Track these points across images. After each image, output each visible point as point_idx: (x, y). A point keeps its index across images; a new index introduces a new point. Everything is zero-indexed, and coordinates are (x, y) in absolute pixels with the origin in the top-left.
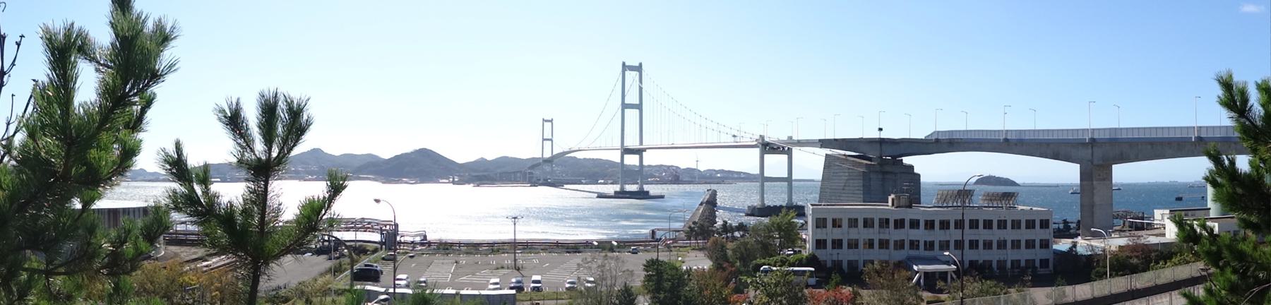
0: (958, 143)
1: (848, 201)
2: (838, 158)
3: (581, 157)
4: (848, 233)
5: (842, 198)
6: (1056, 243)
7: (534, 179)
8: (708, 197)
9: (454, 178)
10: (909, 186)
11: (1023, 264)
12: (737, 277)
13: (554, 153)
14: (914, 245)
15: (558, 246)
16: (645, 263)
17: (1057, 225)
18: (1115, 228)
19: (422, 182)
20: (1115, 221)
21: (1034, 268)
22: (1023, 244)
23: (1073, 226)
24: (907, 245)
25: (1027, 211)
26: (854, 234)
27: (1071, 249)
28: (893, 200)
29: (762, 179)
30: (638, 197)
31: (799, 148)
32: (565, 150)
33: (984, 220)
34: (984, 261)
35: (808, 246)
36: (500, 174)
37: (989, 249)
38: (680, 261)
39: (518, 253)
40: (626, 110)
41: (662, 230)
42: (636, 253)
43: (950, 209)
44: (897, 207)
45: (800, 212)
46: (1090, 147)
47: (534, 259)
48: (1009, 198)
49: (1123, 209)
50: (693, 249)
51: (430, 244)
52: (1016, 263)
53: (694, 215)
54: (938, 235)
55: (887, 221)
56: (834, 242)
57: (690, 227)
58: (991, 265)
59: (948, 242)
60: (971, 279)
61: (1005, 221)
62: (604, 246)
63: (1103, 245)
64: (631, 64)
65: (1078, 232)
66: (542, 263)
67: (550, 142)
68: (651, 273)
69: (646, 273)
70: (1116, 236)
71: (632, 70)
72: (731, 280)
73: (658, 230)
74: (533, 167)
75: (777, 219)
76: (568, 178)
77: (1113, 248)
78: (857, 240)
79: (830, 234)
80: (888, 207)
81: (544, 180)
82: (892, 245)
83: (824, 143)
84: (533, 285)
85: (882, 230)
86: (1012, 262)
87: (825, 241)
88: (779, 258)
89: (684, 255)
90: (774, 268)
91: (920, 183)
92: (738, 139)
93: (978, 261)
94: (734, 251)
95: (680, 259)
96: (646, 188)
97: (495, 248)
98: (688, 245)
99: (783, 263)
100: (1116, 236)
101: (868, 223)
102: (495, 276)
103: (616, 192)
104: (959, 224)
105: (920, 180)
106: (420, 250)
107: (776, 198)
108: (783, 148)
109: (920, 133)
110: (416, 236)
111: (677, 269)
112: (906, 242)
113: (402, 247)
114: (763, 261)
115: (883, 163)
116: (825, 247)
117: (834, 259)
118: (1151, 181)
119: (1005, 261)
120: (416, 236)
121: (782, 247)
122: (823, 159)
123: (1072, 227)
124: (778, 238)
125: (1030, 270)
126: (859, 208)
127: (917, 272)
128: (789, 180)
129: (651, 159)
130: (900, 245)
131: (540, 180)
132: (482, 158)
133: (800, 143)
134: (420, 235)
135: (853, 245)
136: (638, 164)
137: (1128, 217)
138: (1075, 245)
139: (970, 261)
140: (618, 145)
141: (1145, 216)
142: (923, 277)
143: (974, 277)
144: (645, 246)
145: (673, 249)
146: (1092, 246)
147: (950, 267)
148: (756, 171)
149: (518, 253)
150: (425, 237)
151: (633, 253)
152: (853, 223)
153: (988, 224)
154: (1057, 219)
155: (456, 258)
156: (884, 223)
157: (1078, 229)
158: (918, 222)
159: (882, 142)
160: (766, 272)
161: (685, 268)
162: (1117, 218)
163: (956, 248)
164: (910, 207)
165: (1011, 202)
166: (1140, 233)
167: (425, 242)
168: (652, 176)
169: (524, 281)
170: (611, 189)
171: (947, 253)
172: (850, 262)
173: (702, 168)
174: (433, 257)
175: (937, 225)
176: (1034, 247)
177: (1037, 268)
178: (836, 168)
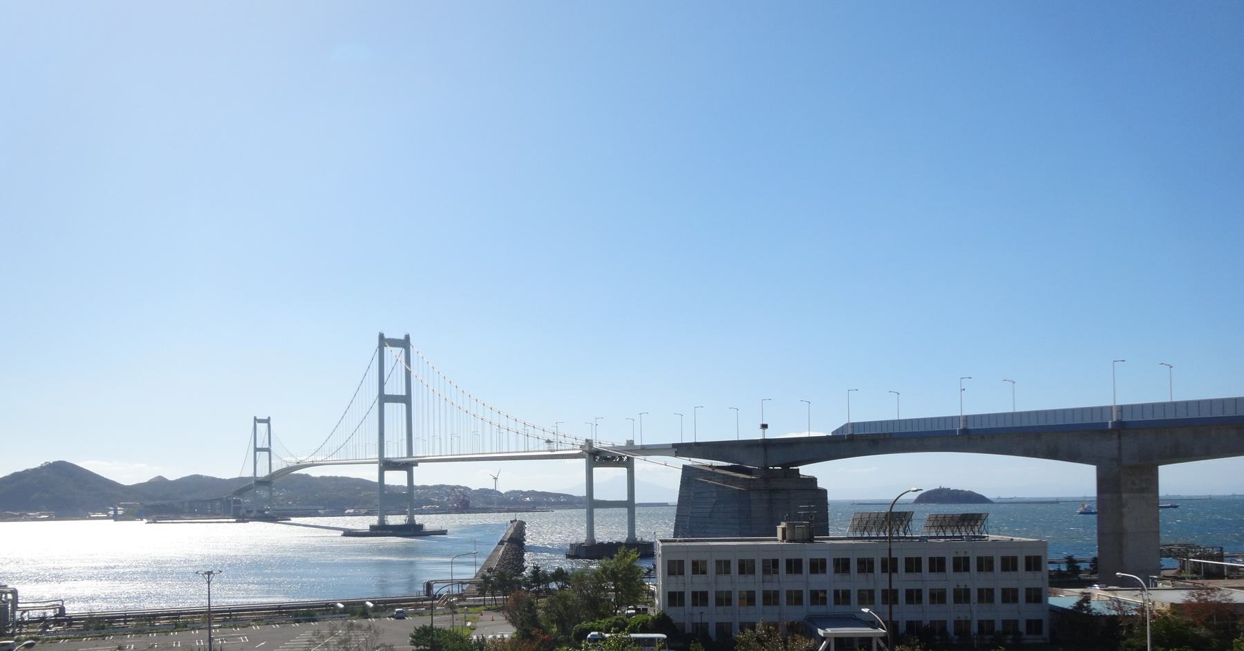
3: (304, 473)
6: (1055, 595)
7: (243, 511)
8: (511, 531)
10: (809, 509)
11: (998, 627)
13: (274, 470)
15: (280, 613)
16: (412, 631)
18: (1164, 573)
21: (1017, 633)
22: (998, 595)
23: (1083, 566)
24: (806, 598)
27: (1080, 604)
28: (784, 530)
29: (590, 504)
30: (409, 533)
31: (642, 457)
32: (290, 465)
33: (931, 559)
35: (657, 602)
37: (939, 603)
39: (215, 628)
40: (386, 405)
41: (442, 581)
42: (403, 618)
44: (790, 541)
45: (646, 550)
46: (1115, 436)
50: (489, 609)
51: (70, 621)
53: (490, 558)
54: (855, 582)
55: (775, 563)
59: (871, 592)
61: (967, 560)
63: (1140, 601)
67: (267, 453)
68: (422, 647)
70: (1166, 586)
71: (395, 346)
73: (436, 582)
74: (240, 492)
76: (299, 507)
78: (729, 593)
79: (690, 583)
80: (777, 541)
81: (259, 511)
83: (680, 449)
85: (768, 577)
86: (981, 623)
87: (682, 594)
90: (607, 635)
91: (827, 504)
92: (554, 446)
93: (921, 622)
95: (469, 624)
96: (419, 519)
99: (621, 626)
100: (1166, 586)
101: (746, 567)
104: (890, 565)
107: (610, 530)
108: (621, 457)
109: (822, 429)
111: (462, 640)
113: (24, 631)
115: (768, 475)
116: (682, 603)
118: (1237, 493)
119: (968, 622)
120: (47, 608)
121: (620, 604)
122: (680, 472)
123: (1082, 569)
124: (612, 591)
125: (1010, 637)
127: (823, 639)
129: (425, 476)
131: (252, 512)
132: (160, 477)
134: (53, 607)
135: (724, 599)
136: (405, 484)
137: (1190, 554)
138: (1087, 598)
140: (375, 455)
141: (1226, 553)
144: (417, 606)
145: (459, 610)
146: (1119, 601)
147: (876, 631)
148: (582, 492)
149: (215, 628)
150: (62, 609)
151: (397, 618)
153: (937, 565)
154: (1055, 558)
155: (120, 642)
156: (771, 566)
158: (823, 562)
159: (767, 444)
161: (475, 637)
163: (885, 601)
164: (811, 540)
165: (976, 528)
166: (1213, 583)
167: (62, 618)
170: (364, 523)
171: (866, 610)
172: (720, 626)
173: (503, 488)
174: (77, 643)
175: (854, 566)
176: (1015, 600)
177: (1021, 633)
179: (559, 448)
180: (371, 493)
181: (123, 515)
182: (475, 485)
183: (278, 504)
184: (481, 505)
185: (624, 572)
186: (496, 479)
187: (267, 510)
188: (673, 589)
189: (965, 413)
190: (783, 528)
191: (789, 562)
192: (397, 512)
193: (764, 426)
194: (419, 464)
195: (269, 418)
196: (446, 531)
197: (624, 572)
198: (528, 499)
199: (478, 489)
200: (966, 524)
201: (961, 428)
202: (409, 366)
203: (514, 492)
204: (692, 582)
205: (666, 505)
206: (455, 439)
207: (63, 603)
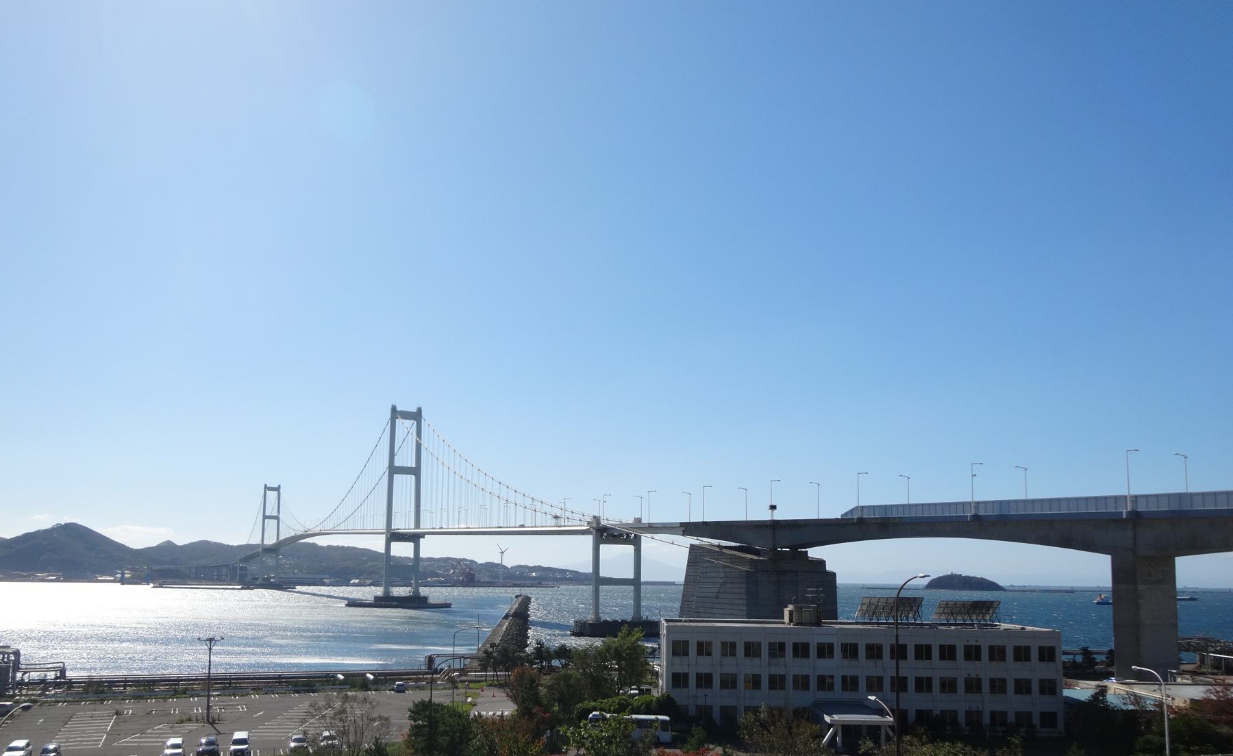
0: (896, 524)
1: (723, 615)
2: (709, 551)
4: (721, 665)
5: (715, 611)
6: (1069, 687)
8: (516, 606)
9: (123, 574)
11: (1011, 718)
12: (554, 727)
14: (824, 683)
17: (1072, 657)
19: (68, 578)
20: (1183, 655)
23: (1099, 658)
24: (813, 683)
25: (1015, 631)
26: (730, 666)
27: (1095, 697)
28: (791, 613)
29: (596, 580)
31: (650, 535)
32: (298, 533)
34: (941, 711)
35: (660, 682)
36: (197, 568)
38: (470, 703)
39: (214, 696)
42: (404, 692)
43: (882, 627)
44: (797, 624)
45: (651, 630)
47: (240, 705)
48: (984, 611)
49: (1201, 635)
50: (491, 685)
51: (70, 684)
52: (998, 718)
53: (494, 632)
54: (863, 668)
55: (782, 646)
56: (699, 677)
57: (486, 652)
58: (956, 717)
60: (915, 741)
62: (356, 680)
63: (1157, 696)
64: (404, 409)
65: (1110, 669)
66: (252, 709)
68: (420, 722)
69: (413, 723)
72: (545, 733)
73: (438, 656)
74: (247, 559)
75: (615, 641)
76: (304, 576)
77: (1179, 703)
79: (694, 665)
82: (789, 683)
83: (688, 529)
84: (233, 747)
87: (686, 676)
88: (617, 699)
89: (476, 694)
93: (932, 711)
94: (550, 688)
95: (469, 700)
96: (424, 591)
97: (178, 687)
98: (483, 678)
101: (752, 650)
102: (175, 735)
103: (377, 598)
105: (836, 581)
106: (53, 696)
107: (616, 607)
108: (628, 535)
109: (833, 510)
110: (49, 670)
111: (460, 716)
112: (811, 678)
113: (24, 692)
114: (593, 704)
115: (776, 557)
116: (686, 685)
117: (699, 704)
119: (980, 713)
120: (49, 670)
121: (623, 683)
124: (616, 670)
125: (1023, 729)
126: (739, 625)
127: (830, 726)
128: (636, 582)
129: (431, 548)
130: (802, 683)
131: (257, 579)
132: (169, 542)
133: (654, 529)
134: (54, 669)
135: (729, 682)
136: (411, 555)
138: (1103, 691)
139: (917, 711)
140: (381, 525)
142: (840, 733)
143: (919, 737)
144: (418, 680)
145: (459, 685)
146: (1135, 695)
148: (588, 569)
149: (214, 696)
150: (63, 671)
152: (729, 649)
153: (948, 653)
154: (1070, 646)
155: (118, 707)
156: (778, 649)
157: (1111, 664)
159: (775, 525)
160: (596, 719)
162: (1187, 650)
164: (818, 623)
165: (988, 617)
167: (62, 681)
168: (435, 575)
169: (219, 742)
171: (872, 698)
172: (724, 710)
173: (510, 562)
175: (862, 652)
176: (1028, 691)
178: (706, 565)
179: (566, 524)
180: (377, 563)
181: (130, 578)
182: (481, 559)
183: (284, 573)
184: (487, 579)
185: (627, 652)
186: (502, 553)
187: (273, 578)
188: (679, 669)
189: (976, 499)
190: (790, 611)
191: (795, 646)
192: (402, 583)
193: (773, 507)
194: (426, 536)
195: (279, 486)
196: (451, 604)
197: (627, 652)
198: (534, 574)
199: (484, 562)
200: (977, 611)
201: (973, 513)
202: (420, 438)
203: (520, 566)
204: (696, 664)
205: (673, 584)
206: (463, 512)
207: (64, 665)
